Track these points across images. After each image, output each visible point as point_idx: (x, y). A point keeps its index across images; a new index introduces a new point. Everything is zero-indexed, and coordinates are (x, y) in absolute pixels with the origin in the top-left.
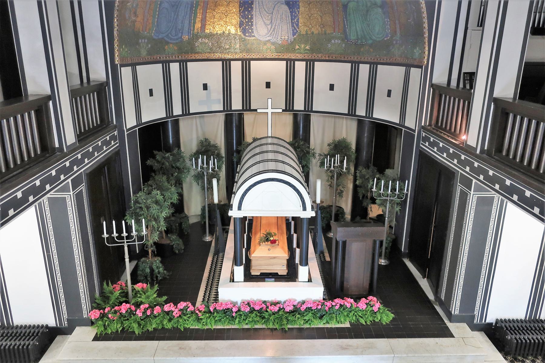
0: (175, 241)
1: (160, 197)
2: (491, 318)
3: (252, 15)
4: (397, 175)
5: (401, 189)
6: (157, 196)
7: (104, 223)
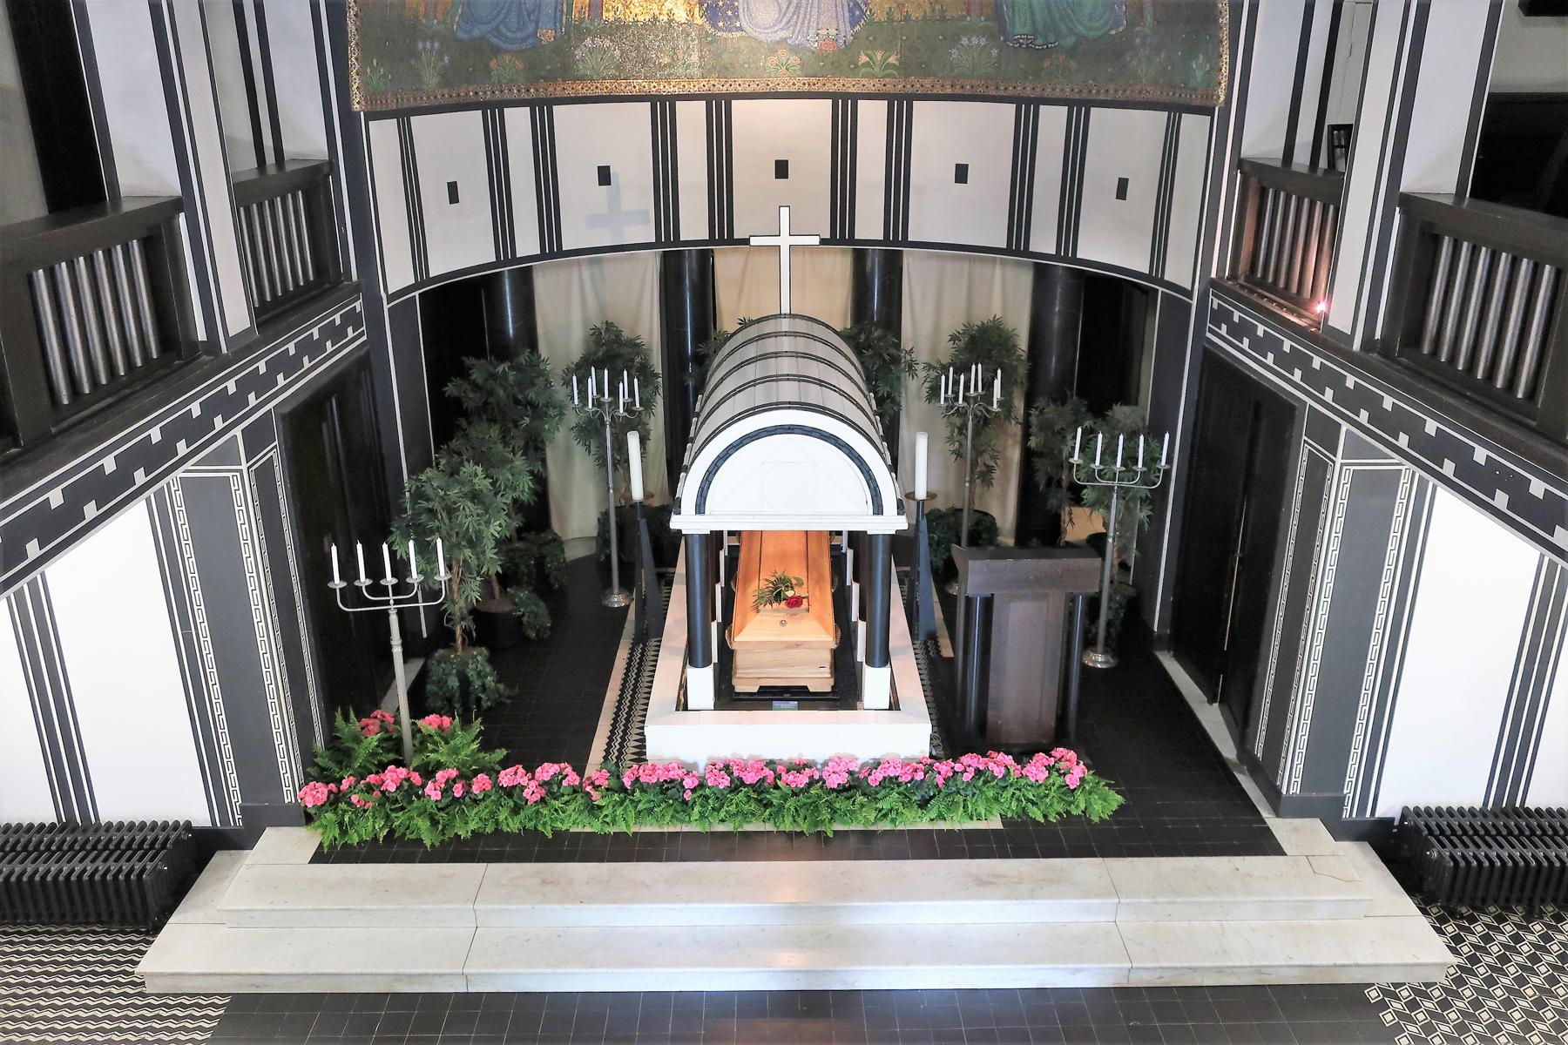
0: (525, 604)
1: (482, 483)
2: (1389, 805)
4: (1143, 419)
5: (1152, 459)
6: (476, 481)
7: (334, 549)
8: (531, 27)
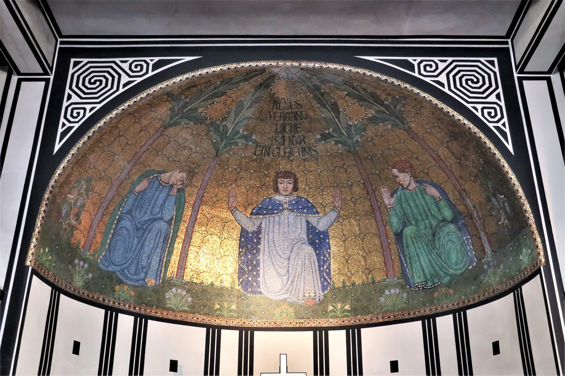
3: (258, 261)
8: (142, 275)
